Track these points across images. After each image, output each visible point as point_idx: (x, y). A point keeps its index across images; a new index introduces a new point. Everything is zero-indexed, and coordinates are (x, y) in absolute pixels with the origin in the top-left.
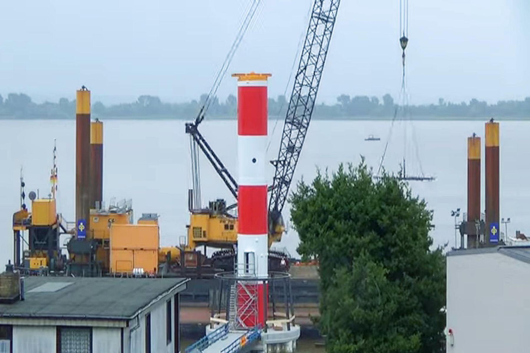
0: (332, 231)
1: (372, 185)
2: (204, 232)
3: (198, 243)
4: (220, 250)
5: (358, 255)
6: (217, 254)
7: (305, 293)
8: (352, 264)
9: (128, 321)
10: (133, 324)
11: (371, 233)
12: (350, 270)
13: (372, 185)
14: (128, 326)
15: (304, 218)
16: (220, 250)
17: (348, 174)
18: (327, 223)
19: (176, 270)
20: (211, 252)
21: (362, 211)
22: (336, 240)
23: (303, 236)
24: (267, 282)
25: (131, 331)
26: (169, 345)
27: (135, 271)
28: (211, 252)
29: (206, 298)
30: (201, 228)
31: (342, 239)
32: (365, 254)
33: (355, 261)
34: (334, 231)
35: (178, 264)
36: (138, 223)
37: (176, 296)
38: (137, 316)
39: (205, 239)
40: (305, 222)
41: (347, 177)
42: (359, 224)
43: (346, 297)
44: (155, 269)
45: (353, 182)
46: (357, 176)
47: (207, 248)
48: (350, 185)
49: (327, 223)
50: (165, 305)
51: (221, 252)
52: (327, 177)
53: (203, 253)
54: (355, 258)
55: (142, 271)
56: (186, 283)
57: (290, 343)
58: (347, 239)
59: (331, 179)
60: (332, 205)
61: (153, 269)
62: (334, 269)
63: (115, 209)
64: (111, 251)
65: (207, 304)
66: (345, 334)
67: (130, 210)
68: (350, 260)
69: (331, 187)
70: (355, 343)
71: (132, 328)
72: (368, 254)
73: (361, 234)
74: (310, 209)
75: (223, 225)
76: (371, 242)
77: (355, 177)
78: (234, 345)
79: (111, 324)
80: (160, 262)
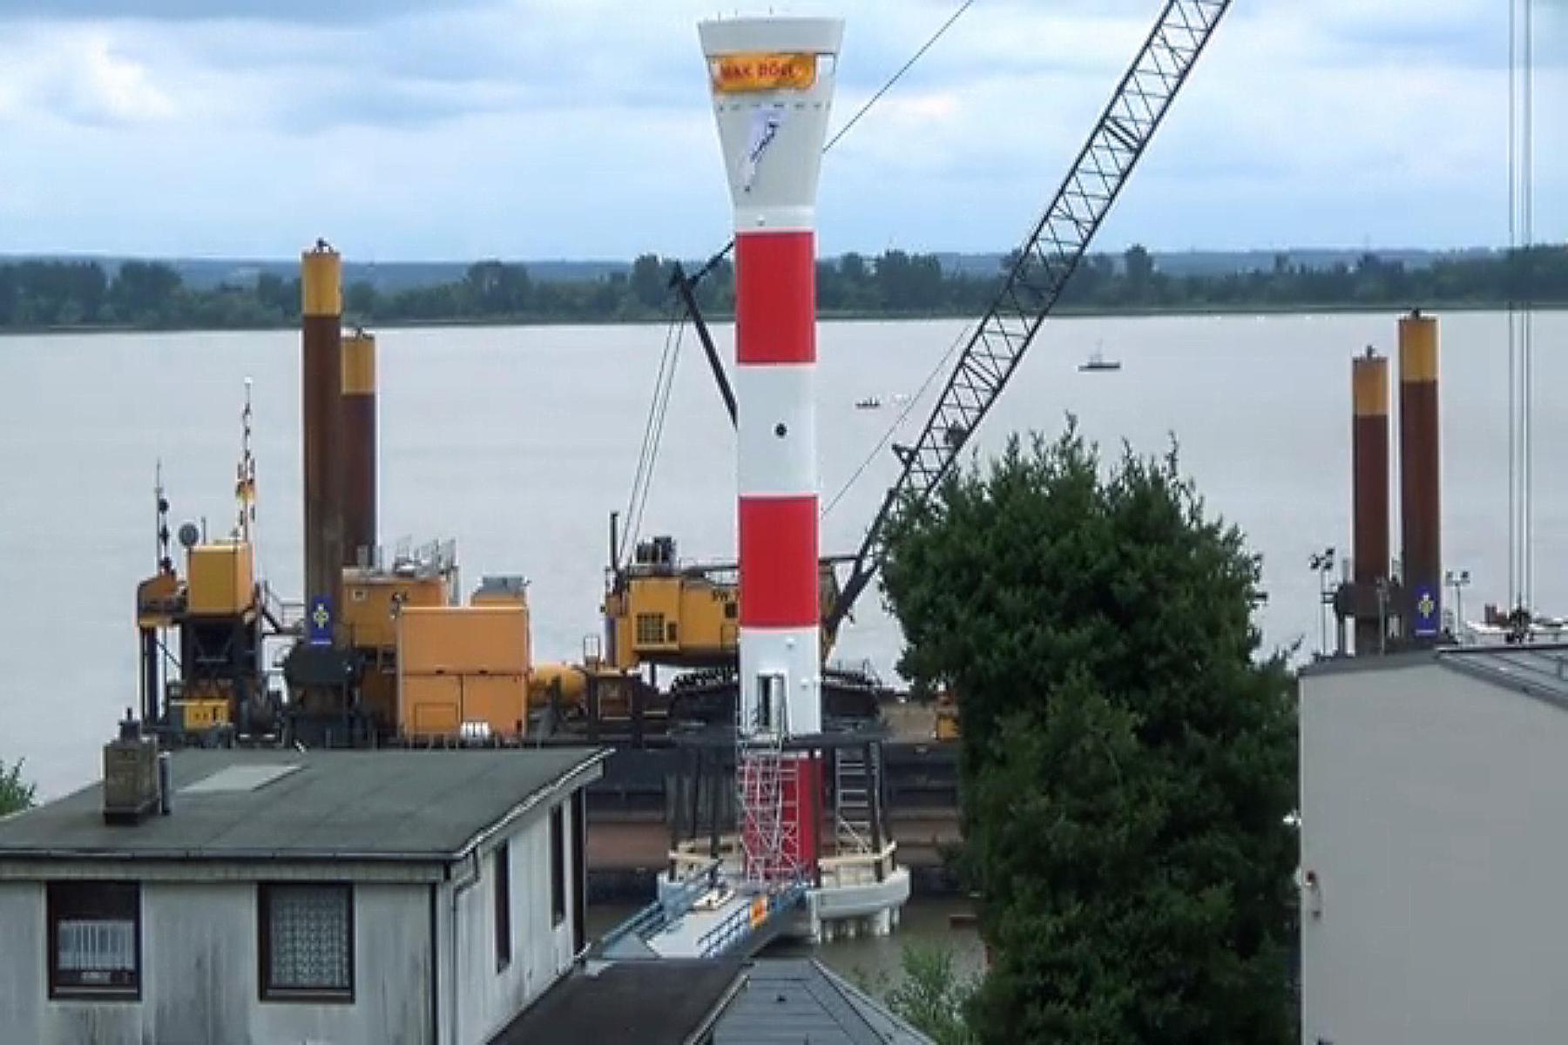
0: (992, 616)
1: (1096, 489)
2: (672, 627)
3: (643, 656)
4: (690, 671)
5: (1060, 679)
6: (680, 683)
7: (921, 781)
8: (1045, 703)
9: (447, 865)
10: (461, 874)
11: (1094, 619)
12: (1042, 717)
13: (1096, 489)
14: (448, 877)
15: (915, 581)
16: (690, 671)
17: (1031, 462)
18: (979, 596)
19: (575, 726)
20: (666, 678)
21: (1071, 561)
22: (1004, 638)
23: (913, 631)
24: (818, 753)
25: (459, 890)
26: (559, 928)
27: (468, 729)
28: (666, 678)
29: (657, 798)
30: (661, 617)
31: (1017, 636)
32: (1079, 675)
33: (1053, 694)
34: (998, 616)
35: (581, 711)
36: (473, 602)
37: (576, 797)
38: (474, 850)
39: (674, 646)
40: (920, 592)
41: (1030, 469)
42: (1064, 594)
43: (1031, 791)
44: (519, 725)
45: (1042, 481)
46: (1057, 467)
47: (659, 668)
48: (1038, 491)
49: (979, 596)
50: (544, 828)
51: (694, 677)
52: (976, 471)
53: (646, 679)
54: (1053, 687)
55: (484, 729)
56: (603, 760)
57: (886, 913)
58: (1031, 636)
59: (986, 476)
60: (989, 545)
61: (513, 726)
62: (997, 719)
63: (409, 567)
64: (401, 680)
65: (659, 816)
66: (1029, 891)
67: (451, 569)
68: (1041, 692)
69: (987, 497)
70: (1057, 912)
71: (459, 881)
72: (1087, 675)
73: (1069, 621)
74: (931, 556)
75: (720, 606)
76: (1097, 641)
77: (1052, 471)
78: (734, 923)
79: (403, 874)
80: (532, 705)
